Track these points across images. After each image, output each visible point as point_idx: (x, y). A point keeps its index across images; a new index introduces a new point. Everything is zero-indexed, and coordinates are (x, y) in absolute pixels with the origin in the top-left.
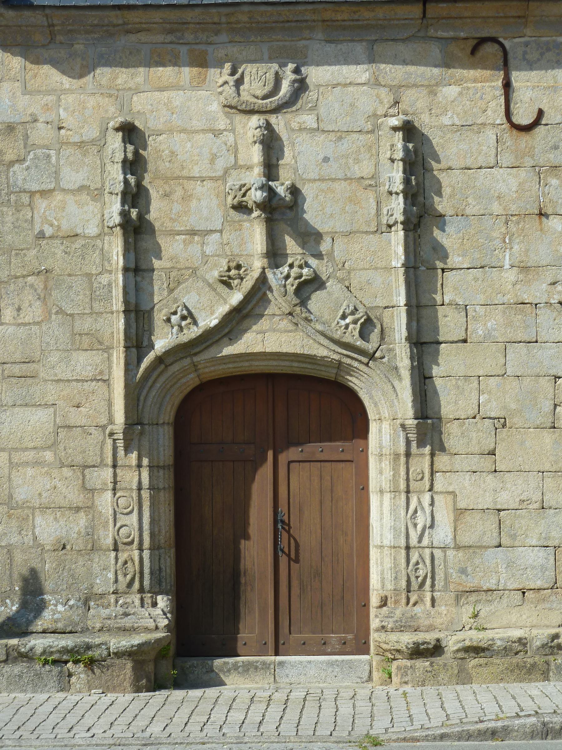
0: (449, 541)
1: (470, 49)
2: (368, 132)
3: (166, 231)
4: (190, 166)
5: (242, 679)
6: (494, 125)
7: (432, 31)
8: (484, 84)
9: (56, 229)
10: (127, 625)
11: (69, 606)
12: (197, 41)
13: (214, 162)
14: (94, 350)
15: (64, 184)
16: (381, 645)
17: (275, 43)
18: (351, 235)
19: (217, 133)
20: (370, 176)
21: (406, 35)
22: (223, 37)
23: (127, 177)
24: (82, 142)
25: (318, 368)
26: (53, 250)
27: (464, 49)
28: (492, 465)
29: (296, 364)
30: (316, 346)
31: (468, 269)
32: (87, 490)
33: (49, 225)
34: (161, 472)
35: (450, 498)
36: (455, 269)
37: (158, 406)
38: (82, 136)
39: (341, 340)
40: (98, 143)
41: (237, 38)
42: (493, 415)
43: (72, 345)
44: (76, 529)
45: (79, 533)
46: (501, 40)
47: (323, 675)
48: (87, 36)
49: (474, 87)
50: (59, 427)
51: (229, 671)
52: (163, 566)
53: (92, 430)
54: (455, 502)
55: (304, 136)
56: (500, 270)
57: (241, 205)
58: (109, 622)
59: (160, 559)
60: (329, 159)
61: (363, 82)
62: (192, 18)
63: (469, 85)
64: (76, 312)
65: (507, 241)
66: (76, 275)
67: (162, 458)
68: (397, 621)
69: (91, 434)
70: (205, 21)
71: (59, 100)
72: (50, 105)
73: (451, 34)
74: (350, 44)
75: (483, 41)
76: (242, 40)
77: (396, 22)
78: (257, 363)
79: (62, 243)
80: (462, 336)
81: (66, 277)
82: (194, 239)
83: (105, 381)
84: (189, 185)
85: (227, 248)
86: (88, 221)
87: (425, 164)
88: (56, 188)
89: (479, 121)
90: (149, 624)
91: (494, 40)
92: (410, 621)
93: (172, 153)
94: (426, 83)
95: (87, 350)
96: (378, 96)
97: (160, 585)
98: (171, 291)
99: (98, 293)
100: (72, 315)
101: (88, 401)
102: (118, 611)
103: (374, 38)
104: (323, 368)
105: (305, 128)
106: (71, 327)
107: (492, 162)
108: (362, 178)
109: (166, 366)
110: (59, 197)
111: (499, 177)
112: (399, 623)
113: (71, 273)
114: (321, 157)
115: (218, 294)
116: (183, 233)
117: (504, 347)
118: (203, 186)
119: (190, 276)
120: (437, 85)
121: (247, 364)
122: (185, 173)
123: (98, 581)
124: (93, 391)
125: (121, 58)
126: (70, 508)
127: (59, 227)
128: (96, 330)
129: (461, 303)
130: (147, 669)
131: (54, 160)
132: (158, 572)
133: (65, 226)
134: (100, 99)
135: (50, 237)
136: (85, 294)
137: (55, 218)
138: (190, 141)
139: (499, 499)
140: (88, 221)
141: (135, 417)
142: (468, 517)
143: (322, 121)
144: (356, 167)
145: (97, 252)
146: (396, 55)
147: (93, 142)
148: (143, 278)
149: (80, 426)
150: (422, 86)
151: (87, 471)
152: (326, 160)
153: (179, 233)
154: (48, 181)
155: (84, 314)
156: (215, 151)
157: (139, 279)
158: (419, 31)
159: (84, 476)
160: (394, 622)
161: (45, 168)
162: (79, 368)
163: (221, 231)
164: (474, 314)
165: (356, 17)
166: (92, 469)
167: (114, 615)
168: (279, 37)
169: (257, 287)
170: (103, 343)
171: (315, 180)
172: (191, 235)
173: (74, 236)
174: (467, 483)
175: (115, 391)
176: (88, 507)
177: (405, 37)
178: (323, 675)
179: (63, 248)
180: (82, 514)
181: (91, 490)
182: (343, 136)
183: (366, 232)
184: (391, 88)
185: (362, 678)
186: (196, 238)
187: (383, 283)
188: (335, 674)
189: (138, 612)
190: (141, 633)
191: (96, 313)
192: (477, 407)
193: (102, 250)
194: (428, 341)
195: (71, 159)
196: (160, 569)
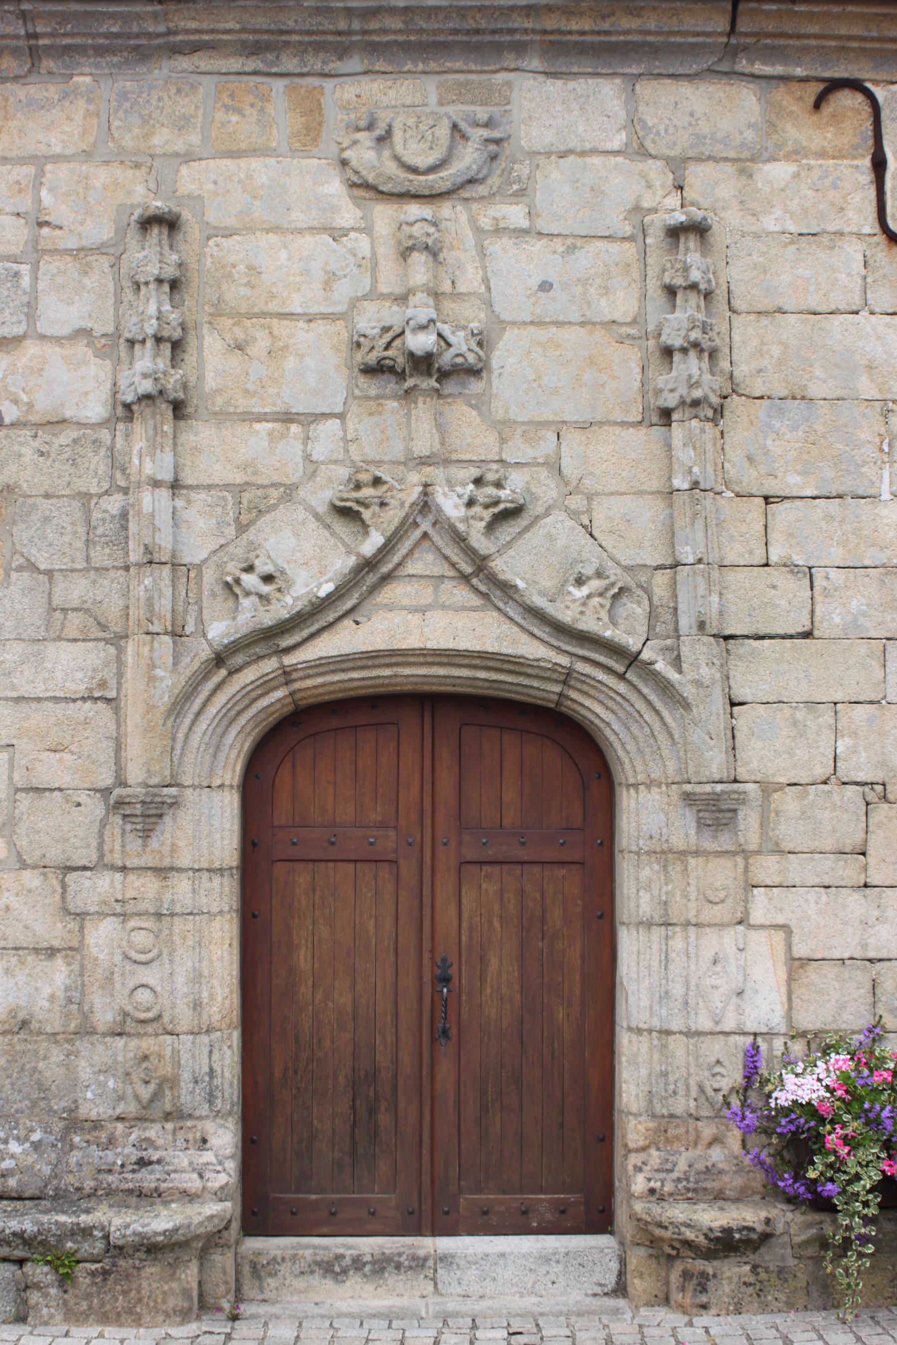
0: (776, 1021)
1: (812, 99)
2: (624, 239)
3: (235, 413)
4: (286, 294)
5: (370, 1287)
6: (859, 235)
7: (744, 62)
8: (840, 162)
9: (25, 408)
10: (146, 1184)
11: (33, 1143)
12: (305, 70)
13: (331, 287)
14: (91, 640)
15: (42, 327)
16: (650, 1228)
17: (451, 77)
18: (592, 428)
19: (337, 234)
20: (629, 320)
21: (695, 68)
22: (354, 63)
23: (163, 309)
24: (82, 249)
25: (526, 681)
26: (16, 447)
27: (801, 98)
28: (860, 874)
29: (482, 674)
30: (525, 637)
31: (814, 498)
32: (70, 914)
33: (11, 401)
34: (217, 880)
35: (780, 935)
36: (788, 498)
37: (211, 750)
38: (81, 238)
39: (575, 626)
40: (112, 251)
41: (380, 66)
42: (861, 777)
43: (47, 630)
44: (47, 991)
45: (52, 998)
46: (868, 85)
47: (530, 1280)
48: (99, 59)
49: (821, 165)
50: (18, 790)
51: (345, 1271)
52: (215, 1066)
53: (83, 797)
54: (789, 946)
55: (506, 242)
56: (872, 503)
57: (382, 366)
58: (110, 1178)
59: (211, 1052)
60: (551, 285)
61: (616, 148)
62: (296, 21)
63: (812, 162)
64: (57, 567)
65: (886, 449)
66: (58, 497)
67: (217, 853)
68: (679, 1180)
69: (79, 805)
70: (321, 28)
71: (41, 173)
72: (23, 184)
73: (779, 70)
74: (590, 81)
75: (834, 85)
76: (390, 69)
77: (678, 39)
78: (407, 671)
79: (35, 436)
80: (764, 562)
81: (40, 500)
82: (288, 429)
83: (108, 701)
84: (282, 328)
85: (352, 448)
86: (86, 394)
87: (732, 301)
88: (30, 333)
89: (831, 228)
90: (190, 1184)
91: (856, 85)
92: (705, 1180)
93: (250, 268)
94: (732, 154)
95: (75, 640)
96: (644, 175)
97: (211, 1103)
98: (242, 528)
99: (100, 531)
100: (49, 573)
101: (76, 739)
102: (128, 1156)
103: (635, 71)
104: (536, 683)
105: (504, 229)
106: (46, 595)
107: (856, 301)
108: (614, 322)
109: (230, 674)
110: (32, 348)
111: (868, 329)
112: (684, 1183)
113: (50, 491)
114: (535, 282)
115: (334, 534)
116: (268, 417)
117: (882, 648)
118: (308, 331)
119: (280, 499)
120: (753, 159)
121: (387, 672)
122: (273, 307)
123: (89, 1095)
124: (86, 719)
125: (160, 99)
126: (37, 950)
127: (30, 405)
128: (95, 602)
129: (801, 563)
130: (183, 1276)
131: (26, 281)
132: (207, 1079)
133: (43, 405)
134: (119, 171)
135: (12, 425)
136: (75, 533)
137: (23, 390)
138: (285, 247)
139: (871, 941)
140: (86, 394)
141: (167, 773)
142: (812, 974)
143: (538, 216)
144: (603, 302)
145: (103, 451)
146: (676, 103)
147: (100, 249)
148: (189, 502)
149: (60, 789)
150: (726, 159)
151: (72, 877)
152: (545, 286)
153: (261, 418)
154: (14, 319)
155: (73, 571)
156: (332, 266)
157: (180, 503)
158: (720, 60)
159: (64, 886)
160: (673, 1181)
161: (8, 296)
162: (59, 675)
163: (341, 416)
164: (825, 583)
165: (606, 26)
166: (80, 873)
167: (119, 1162)
168: (458, 64)
169: (411, 520)
170: (107, 627)
171: (524, 323)
172: (284, 421)
173: (57, 422)
174: (812, 909)
175: (128, 721)
176: (70, 948)
177: (692, 71)
178: (530, 1280)
179: (36, 444)
180: (59, 961)
181: (78, 915)
182: (579, 244)
183: (623, 424)
184: (668, 160)
185: (604, 1285)
186: (294, 428)
187: (654, 521)
188: (552, 1277)
189: (168, 1159)
190: (172, 1201)
191: (96, 569)
192: (832, 763)
193: (111, 449)
194: (738, 633)
195: (59, 280)
196: (212, 1072)
